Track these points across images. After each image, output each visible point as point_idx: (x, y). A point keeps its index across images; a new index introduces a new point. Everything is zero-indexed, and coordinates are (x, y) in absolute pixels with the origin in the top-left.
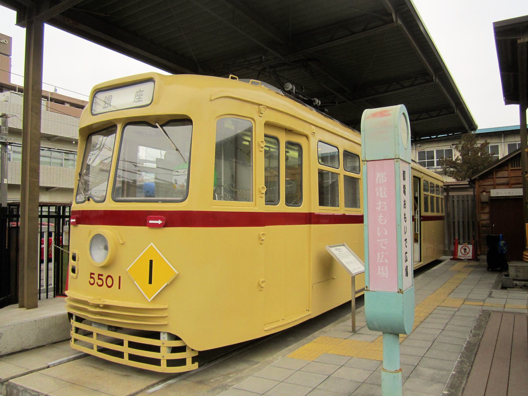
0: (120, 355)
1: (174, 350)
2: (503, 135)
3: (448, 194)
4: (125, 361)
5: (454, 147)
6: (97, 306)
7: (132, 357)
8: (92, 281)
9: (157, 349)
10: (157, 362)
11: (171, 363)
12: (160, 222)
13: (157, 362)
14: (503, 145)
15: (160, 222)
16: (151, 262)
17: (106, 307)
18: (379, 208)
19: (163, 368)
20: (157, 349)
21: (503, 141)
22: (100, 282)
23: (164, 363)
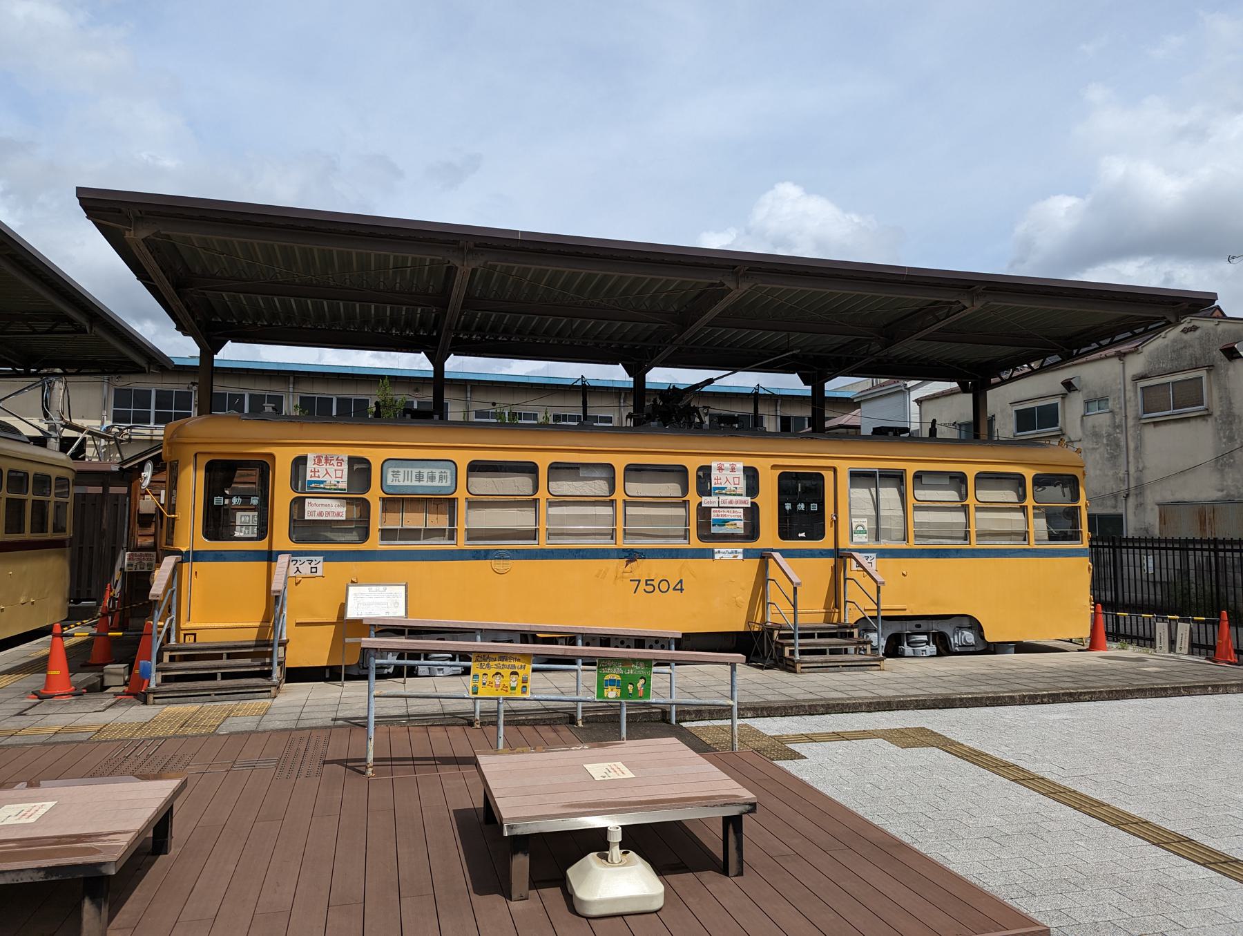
2: (291, 379)
3: (105, 490)
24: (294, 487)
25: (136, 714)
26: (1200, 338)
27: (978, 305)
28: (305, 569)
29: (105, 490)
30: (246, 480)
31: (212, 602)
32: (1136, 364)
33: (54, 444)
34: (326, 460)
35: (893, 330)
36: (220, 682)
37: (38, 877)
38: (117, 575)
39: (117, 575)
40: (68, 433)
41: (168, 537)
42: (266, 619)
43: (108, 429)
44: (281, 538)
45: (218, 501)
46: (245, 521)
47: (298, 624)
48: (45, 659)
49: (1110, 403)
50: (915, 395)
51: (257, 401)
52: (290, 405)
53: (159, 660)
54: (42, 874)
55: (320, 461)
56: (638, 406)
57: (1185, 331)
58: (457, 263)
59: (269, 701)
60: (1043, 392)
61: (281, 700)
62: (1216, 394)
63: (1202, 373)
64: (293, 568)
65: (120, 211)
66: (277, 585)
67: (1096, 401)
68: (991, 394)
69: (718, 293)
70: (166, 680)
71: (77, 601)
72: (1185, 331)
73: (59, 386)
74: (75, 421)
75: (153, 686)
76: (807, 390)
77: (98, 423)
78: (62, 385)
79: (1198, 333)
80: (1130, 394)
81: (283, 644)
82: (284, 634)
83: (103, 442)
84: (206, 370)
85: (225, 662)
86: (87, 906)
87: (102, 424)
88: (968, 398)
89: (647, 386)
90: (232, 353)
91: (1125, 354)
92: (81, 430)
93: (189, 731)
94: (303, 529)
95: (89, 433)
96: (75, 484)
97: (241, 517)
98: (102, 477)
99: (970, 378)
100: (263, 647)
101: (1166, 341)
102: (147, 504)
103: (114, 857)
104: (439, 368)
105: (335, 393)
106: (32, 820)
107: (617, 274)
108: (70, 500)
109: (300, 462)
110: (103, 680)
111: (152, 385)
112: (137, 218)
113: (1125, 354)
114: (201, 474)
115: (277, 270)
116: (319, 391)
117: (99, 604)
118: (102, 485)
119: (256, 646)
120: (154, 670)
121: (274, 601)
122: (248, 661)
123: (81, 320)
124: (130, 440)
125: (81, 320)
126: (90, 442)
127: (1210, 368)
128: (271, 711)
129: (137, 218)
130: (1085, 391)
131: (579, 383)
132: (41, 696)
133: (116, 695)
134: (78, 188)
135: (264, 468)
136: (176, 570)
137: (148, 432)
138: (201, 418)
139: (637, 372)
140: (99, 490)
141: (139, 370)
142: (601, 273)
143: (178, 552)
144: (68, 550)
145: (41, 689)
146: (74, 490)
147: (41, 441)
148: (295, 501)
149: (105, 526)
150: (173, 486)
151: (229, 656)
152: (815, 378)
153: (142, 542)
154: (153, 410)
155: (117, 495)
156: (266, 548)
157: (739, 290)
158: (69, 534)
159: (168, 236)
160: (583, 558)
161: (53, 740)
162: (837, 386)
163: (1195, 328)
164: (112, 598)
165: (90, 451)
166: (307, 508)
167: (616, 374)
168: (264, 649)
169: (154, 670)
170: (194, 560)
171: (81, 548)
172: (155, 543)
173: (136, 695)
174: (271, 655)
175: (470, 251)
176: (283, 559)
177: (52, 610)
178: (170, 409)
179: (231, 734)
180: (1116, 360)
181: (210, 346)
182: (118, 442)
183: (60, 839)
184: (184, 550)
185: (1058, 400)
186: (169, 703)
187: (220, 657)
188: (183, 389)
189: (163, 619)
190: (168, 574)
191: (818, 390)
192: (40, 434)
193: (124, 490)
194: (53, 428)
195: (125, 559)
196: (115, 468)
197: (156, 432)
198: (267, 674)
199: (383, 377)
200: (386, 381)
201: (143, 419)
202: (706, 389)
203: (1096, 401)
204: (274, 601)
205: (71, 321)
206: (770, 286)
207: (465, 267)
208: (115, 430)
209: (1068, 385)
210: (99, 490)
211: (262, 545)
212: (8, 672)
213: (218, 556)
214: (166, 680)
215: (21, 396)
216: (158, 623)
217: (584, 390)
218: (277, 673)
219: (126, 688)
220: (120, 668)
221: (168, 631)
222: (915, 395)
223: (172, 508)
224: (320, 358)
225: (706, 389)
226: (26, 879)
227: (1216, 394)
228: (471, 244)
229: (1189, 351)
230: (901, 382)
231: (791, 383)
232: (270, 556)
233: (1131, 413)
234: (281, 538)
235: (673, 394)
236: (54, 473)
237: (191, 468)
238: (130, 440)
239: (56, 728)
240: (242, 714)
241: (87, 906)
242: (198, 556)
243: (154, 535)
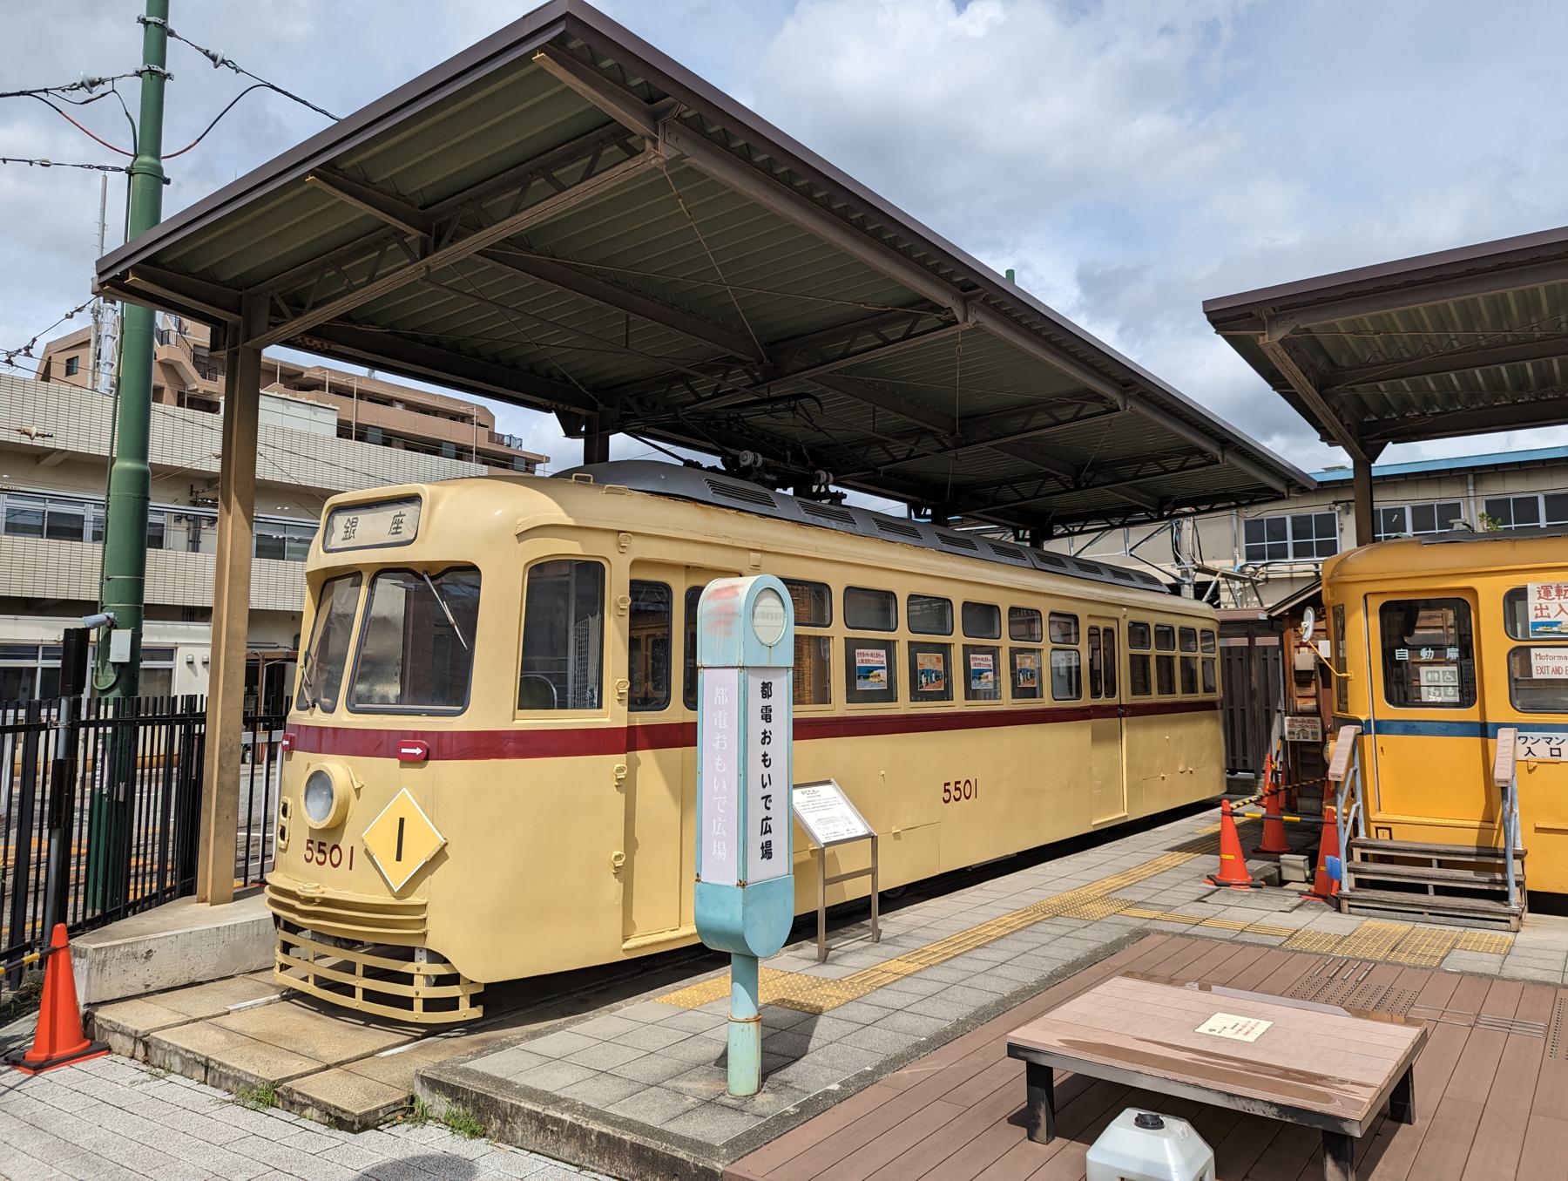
0: (349, 991)
1: (441, 981)
2: (1471, 478)
3: (1251, 641)
4: (357, 1003)
5: (1338, 508)
6: (310, 901)
7: (369, 995)
8: (947, 796)
9: (408, 979)
10: (407, 1003)
11: (431, 1005)
12: (418, 751)
13: (407, 1003)
14: (1472, 503)
15: (418, 751)
16: (402, 820)
17: (326, 902)
18: (717, 745)
19: (417, 1014)
20: (408, 979)
21: (1471, 493)
22: (321, 858)
23: (418, 1004)
24: (1512, 633)
25: (1323, 923)
28: (1542, 750)
29: (1251, 641)
30: (1432, 625)
31: (1410, 788)
33: (1188, 591)
34: (1559, 590)
36: (1431, 898)
37: (1271, 1113)
38: (1276, 745)
39: (1276, 745)
40: (1201, 577)
41: (1340, 701)
42: (1489, 818)
43: (1242, 569)
44: (1497, 701)
45: (1402, 654)
46: (1438, 681)
47: (1538, 830)
48: (1216, 837)
51: (1423, 517)
52: (1473, 513)
53: (1350, 857)
54: (1274, 1110)
55: (1548, 593)
59: (1510, 936)
61: (1525, 937)
64: (1522, 750)
65: (1251, 315)
66: (1502, 772)
70: (1360, 884)
71: (1232, 772)
73: (1187, 524)
74: (1208, 564)
75: (1345, 890)
77: (1230, 563)
78: (1190, 525)
81: (1519, 856)
82: (1519, 842)
83: (1238, 585)
84: (1365, 483)
85: (1434, 871)
86: (1330, 1164)
90: (1395, 456)
92: (1214, 573)
93: (1403, 958)
94: (1530, 691)
95: (1223, 575)
96: (1221, 636)
97: (1426, 675)
98: (1248, 627)
100: (1489, 858)
102: (1303, 660)
103: (1358, 1115)
105: (1540, 488)
106: (1251, 1038)
108: (1217, 655)
109: (1516, 597)
110: (1280, 872)
111: (1286, 511)
112: (1271, 318)
114: (1375, 620)
115: (1452, 335)
116: (1514, 489)
117: (1258, 777)
118: (1247, 635)
119: (1478, 855)
120: (1344, 870)
121: (1498, 794)
122: (1470, 874)
124: (1267, 580)
125: (1212, 448)
126: (1223, 586)
128: (1515, 951)
132: (1219, 883)
133: (1301, 894)
134: (1205, 303)
135: (1462, 606)
136: (1357, 745)
137: (1286, 568)
138: (1364, 549)
140: (1244, 642)
141: (1278, 497)
143: (1356, 722)
144: (1219, 713)
145: (1216, 873)
146: (1220, 643)
147: (1175, 590)
148: (1514, 652)
149: (1255, 684)
150: (1338, 636)
151: (1441, 864)
153: (1303, 704)
154: (1290, 541)
156: (1477, 719)
158: (1218, 695)
159: (1308, 330)
161: (1240, 938)
164: (1275, 772)
165: (1225, 597)
166: (1535, 662)
168: (1492, 860)
169: (1344, 870)
170: (1378, 732)
171: (1231, 711)
172: (1318, 706)
173: (1325, 898)
174: (1503, 869)
176: (1506, 735)
177: (1210, 783)
178: (1316, 537)
179: (1463, 974)
181: (1365, 453)
182: (1254, 583)
183: (1287, 1073)
184: (1363, 718)
186: (1370, 916)
187: (1428, 863)
188: (1324, 511)
189: (1349, 805)
190: (1348, 749)
192: (1173, 581)
193: (1274, 641)
194: (1185, 573)
195: (1284, 727)
196: (1263, 616)
197: (1296, 568)
198: (1503, 897)
201: (1279, 553)
204: (1498, 794)
205: (1202, 452)
208: (1249, 569)
210: (1244, 642)
211: (1471, 714)
212: (1172, 849)
213: (1410, 728)
214: (1360, 884)
215: (1151, 541)
216: (1340, 809)
218: (1516, 899)
219: (1312, 887)
220: (1300, 860)
221: (1355, 820)
223: (1342, 664)
224: (1509, 443)
226: (1258, 1110)
232: (1485, 731)
234: (1497, 701)
236: (1199, 625)
237: (1362, 613)
238: (1267, 580)
239: (1242, 925)
240: (1475, 947)
241: (1330, 1164)
242: (1382, 727)
243: (1316, 697)
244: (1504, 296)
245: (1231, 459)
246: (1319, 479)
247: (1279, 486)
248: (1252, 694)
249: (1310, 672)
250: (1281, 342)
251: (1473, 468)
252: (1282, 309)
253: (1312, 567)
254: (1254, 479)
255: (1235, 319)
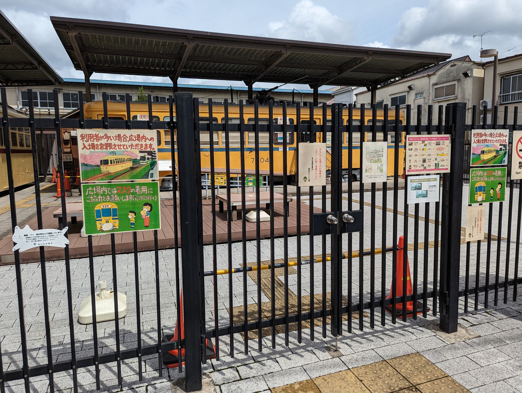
2: (98, 87)
3: (42, 132)
26: (456, 69)
27: (370, 59)
29: (42, 132)
32: (434, 79)
35: (341, 68)
49: (424, 95)
50: (355, 92)
56: (250, 97)
57: (451, 66)
58: (187, 44)
60: (401, 90)
62: (460, 91)
63: (456, 82)
67: (419, 94)
68: (378, 92)
69: (280, 54)
72: (451, 66)
76: (311, 91)
79: (456, 66)
80: (431, 91)
87: (18, 107)
88: (370, 94)
89: (178, 86)
91: (430, 75)
99: (370, 85)
101: (445, 70)
104: (175, 83)
105: (117, 93)
107: (243, 48)
112: (72, 28)
113: (430, 75)
116: (110, 92)
123: (36, 63)
125: (36, 63)
127: (459, 80)
129: (72, 28)
130: (416, 90)
131: (230, 89)
137: (38, 110)
139: (249, 84)
142: (237, 47)
149: (43, 146)
152: (315, 86)
153: (66, 150)
154: (39, 101)
155: (47, 134)
157: (286, 54)
160: (235, 151)
162: (323, 89)
163: (455, 65)
167: (240, 85)
175: (191, 40)
180: (427, 78)
185: (406, 94)
191: (316, 91)
197: (41, 110)
199: (141, 86)
200: (142, 88)
202: (275, 90)
203: (419, 94)
205: (31, 64)
206: (297, 52)
207: (190, 46)
208: (24, 110)
209: (410, 88)
217: (232, 92)
222: (355, 92)
225: (275, 90)
227: (460, 91)
228: (192, 37)
229: (452, 74)
230: (350, 87)
231: (306, 88)
233: (431, 99)
235: (264, 92)
243: (70, 148)
244: (118, 38)
245: (41, 69)
246: (65, 80)
247: (53, 80)
248: (43, 150)
249: (68, 140)
250: (75, 36)
251: (98, 84)
252: (75, 26)
253: (47, 110)
254: (47, 77)
255: (59, 24)
